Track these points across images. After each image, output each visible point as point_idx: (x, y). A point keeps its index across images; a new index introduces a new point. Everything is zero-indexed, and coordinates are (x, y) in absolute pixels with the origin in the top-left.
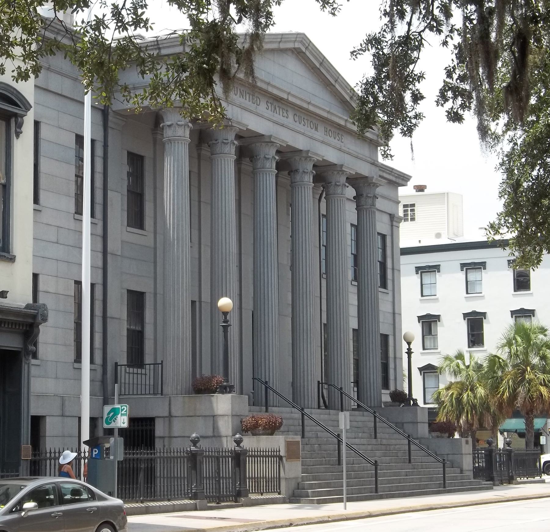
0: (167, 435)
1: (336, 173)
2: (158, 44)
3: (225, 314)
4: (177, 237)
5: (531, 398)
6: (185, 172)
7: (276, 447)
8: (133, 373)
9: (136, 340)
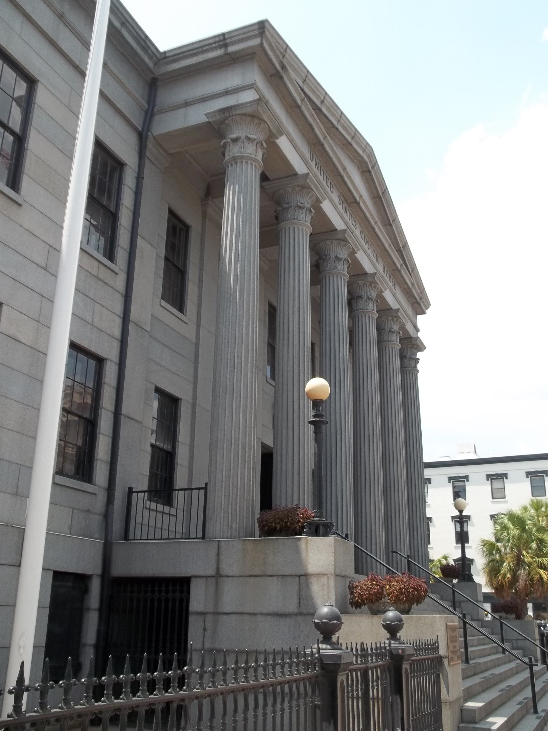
0: (210, 609)
1: (390, 318)
2: (225, 39)
3: (317, 403)
4: (240, 288)
5: (532, 580)
6: (255, 202)
7: (427, 637)
8: (156, 511)
9: (164, 463)
